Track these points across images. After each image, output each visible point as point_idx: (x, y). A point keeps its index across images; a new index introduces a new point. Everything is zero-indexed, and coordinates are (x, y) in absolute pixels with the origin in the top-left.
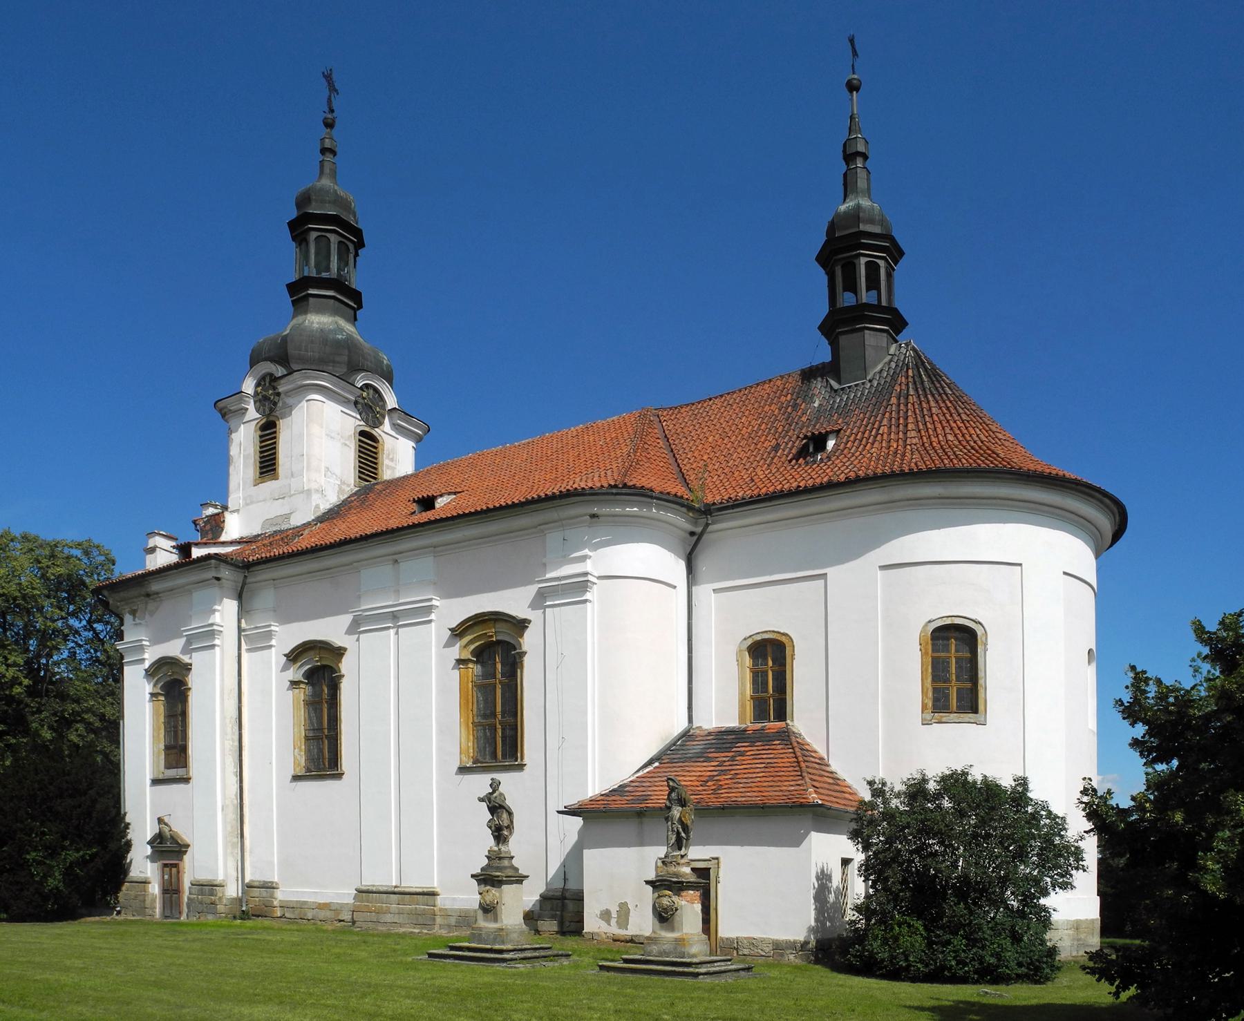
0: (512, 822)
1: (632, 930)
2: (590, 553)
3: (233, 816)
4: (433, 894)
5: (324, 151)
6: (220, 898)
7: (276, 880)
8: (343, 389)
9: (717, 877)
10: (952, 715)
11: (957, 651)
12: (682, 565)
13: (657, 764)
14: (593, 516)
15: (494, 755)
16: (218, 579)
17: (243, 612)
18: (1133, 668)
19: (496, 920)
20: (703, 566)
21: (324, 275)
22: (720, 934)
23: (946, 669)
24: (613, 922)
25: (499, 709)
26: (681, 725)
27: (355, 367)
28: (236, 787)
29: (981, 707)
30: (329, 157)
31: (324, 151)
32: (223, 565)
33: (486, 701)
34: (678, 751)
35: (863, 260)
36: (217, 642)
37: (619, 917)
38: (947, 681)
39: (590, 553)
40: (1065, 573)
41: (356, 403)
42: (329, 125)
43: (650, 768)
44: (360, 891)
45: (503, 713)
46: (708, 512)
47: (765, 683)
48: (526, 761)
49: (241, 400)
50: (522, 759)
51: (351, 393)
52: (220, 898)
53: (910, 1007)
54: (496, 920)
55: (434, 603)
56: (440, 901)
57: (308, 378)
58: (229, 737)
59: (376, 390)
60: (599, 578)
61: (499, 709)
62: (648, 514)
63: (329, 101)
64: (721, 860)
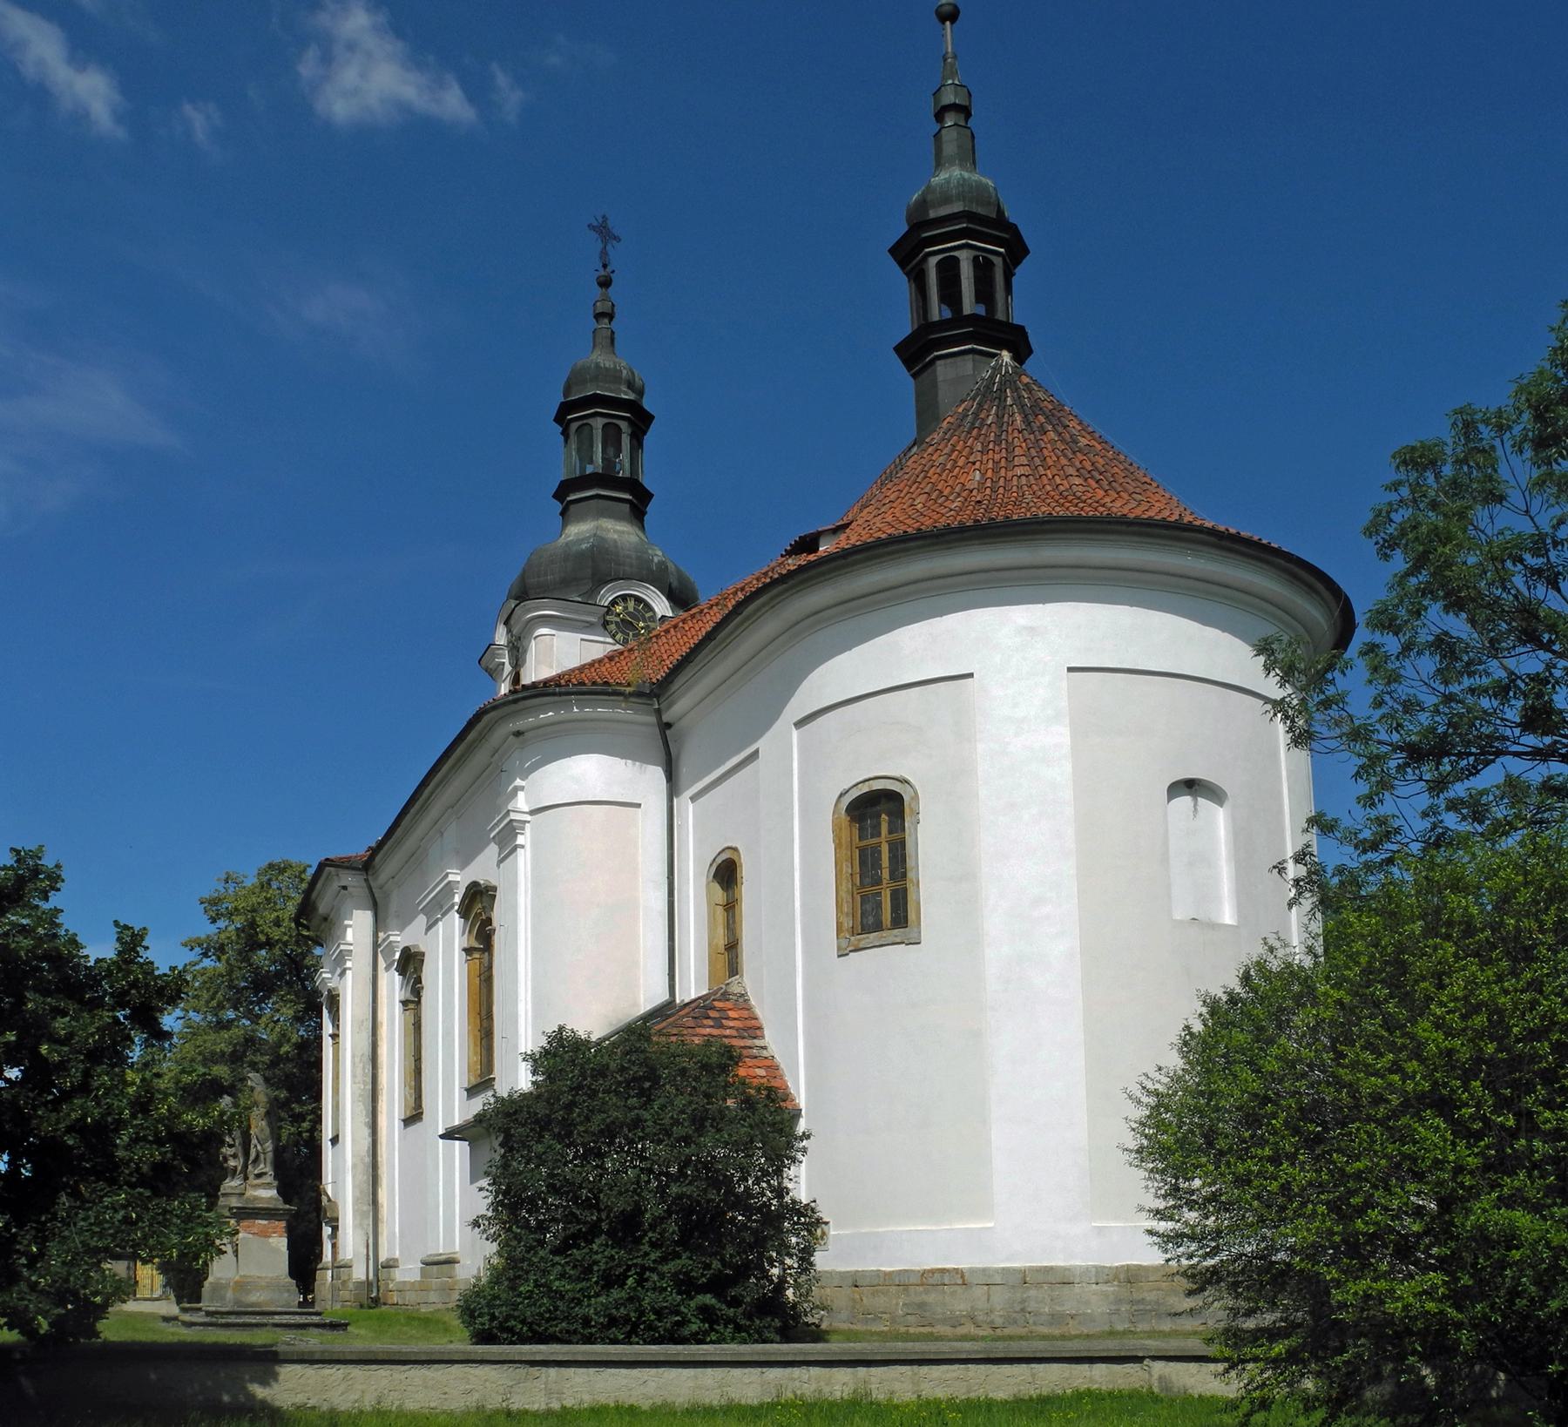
2: (523, 783)
3: (365, 1178)
4: (451, 1261)
5: (598, 316)
6: (344, 1282)
7: (397, 1255)
8: (576, 612)
10: (884, 934)
11: (890, 832)
12: (656, 774)
14: (518, 734)
16: (345, 888)
17: (379, 924)
18: (116, 923)
20: (684, 770)
21: (589, 469)
23: (877, 864)
26: (664, 997)
27: (601, 580)
28: (366, 1142)
29: (912, 916)
30: (605, 322)
31: (598, 316)
32: (342, 873)
35: (933, 261)
36: (349, 964)
38: (878, 881)
39: (523, 783)
40: (1070, 670)
41: (605, 624)
42: (605, 283)
46: (655, 693)
49: (494, 656)
51: (589, 614)
52: (344, 1282)
55: (451, 878)
57: (530, 611)
58: (359, 1078)
59: (638, 600)
60: (533, 812)
62: (568, 716)
63: (604, 253)
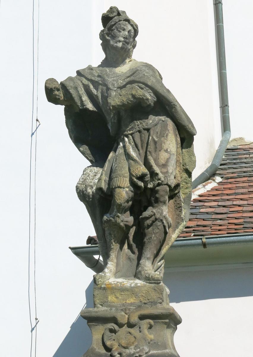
13: (218, 179)
43: (211, 185)
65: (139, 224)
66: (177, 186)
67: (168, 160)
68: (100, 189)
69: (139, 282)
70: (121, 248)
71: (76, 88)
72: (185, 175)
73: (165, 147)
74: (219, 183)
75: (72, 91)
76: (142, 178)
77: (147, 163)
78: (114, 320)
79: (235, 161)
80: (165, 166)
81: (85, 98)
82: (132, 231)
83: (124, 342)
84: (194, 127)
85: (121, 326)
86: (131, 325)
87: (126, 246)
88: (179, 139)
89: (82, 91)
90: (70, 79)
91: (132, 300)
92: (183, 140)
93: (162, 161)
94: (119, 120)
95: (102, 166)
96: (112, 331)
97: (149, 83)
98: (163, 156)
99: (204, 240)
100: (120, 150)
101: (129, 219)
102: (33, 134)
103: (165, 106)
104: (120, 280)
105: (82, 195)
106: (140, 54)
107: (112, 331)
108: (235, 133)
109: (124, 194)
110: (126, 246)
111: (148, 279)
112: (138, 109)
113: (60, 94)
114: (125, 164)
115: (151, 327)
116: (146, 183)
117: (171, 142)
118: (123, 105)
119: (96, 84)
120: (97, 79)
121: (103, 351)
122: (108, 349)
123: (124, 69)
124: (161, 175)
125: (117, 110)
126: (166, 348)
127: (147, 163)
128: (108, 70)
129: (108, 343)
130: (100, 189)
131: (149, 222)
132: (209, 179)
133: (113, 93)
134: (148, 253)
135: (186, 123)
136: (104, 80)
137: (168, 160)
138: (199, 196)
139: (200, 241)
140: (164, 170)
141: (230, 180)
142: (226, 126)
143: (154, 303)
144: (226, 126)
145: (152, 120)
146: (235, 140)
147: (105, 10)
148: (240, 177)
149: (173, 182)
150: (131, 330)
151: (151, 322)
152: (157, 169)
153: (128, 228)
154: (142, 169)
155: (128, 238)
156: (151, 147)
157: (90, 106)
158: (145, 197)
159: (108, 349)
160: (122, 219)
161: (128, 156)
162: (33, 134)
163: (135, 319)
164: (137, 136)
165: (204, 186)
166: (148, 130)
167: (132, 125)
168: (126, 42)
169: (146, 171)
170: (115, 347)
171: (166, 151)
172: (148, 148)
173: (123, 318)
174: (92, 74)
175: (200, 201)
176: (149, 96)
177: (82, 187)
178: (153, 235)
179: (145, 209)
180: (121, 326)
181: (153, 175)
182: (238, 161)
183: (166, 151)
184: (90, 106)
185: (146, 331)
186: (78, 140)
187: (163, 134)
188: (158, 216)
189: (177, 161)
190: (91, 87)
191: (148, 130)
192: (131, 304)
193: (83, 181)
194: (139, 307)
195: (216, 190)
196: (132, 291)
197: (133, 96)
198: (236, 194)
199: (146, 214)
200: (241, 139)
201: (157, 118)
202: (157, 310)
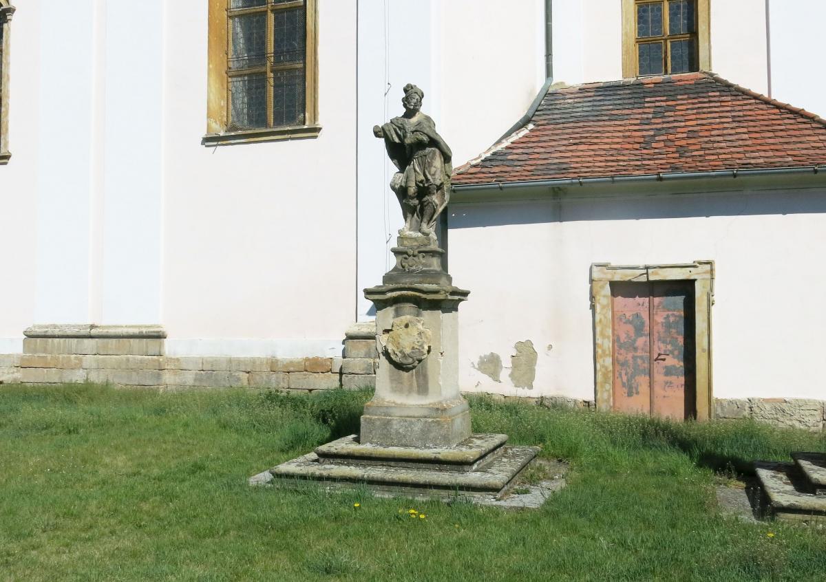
0: (51, 325)
1: (544, 385)
4: (159, 336)
9: (710, 295)
13: (531, 126)
15: (262, 121)
19: (423, 389)
22: (717, 394)
24: (505, 374)
25: (271, 48)
33: (248, 39)
34: (549, 110)
37: (515, 366)
43: (524, 132)
44: (30, 336)
45: (277, 53)
47: (658, 21)
48: (320, 123)
50: (315, 118)
53: (185, 370)
54: (423, 389)
56: (171, 348)
61: (271, 48)
64: (717, 267)
65: (421, 203)
66: (442, 184)
67: (435, 172)
68: (401, 186)
69: (420, 234)
70: (413, 216)
71: (389, 131)
72: (447, 177)
73: (434, 165)
74: (532, 131)
75: (387, 132)
76: (421, 182)
77: (425, 175)
78: (406, 253)
79: (550, 107)
80: (434, 175)
81: (394, 136)
82: (419, 207)
83: (410, 264)
84: (451, 152)
85: (409, 256)
86: (414, 256)
87: (415, 215)
88: (443, 160)
89: (393, 132)
90: (387, 124)
91: (415, 244)
92: (445, 159)
93: (432, 172)
94: (412, 149)
95: (403, 173)
96: (406, 258)
97: (426, 132)
98: (433, 170)
99: (501, 185)
100: (412, 166)
101: (416, 202)
102: (386, 94)
103: (434, 142)
104: (411, 233)
105: (393, 188)
106: (424, 110)
107: (406, 258)
108: (557, 78)
109: (412, 190)
110: (415, 215)
111: (424, 233)
112: (420, 145)
113: (382, 134)
114: (413, 174)
115: (424, 257)
116: (424, 185)
117: (438, 162)
118: (412, 143)
119: (400, 128)
120: (400, 126)
121: (401, 268)
122: (403, 267)
123: (414, 120)
124: (431, 180)
125: (411, 145)
126: (430, 267)
127: (425, 175)
128: (406, 120)
129: (404, 264)
130: (401, 186)
131: (426, 203)
132: (522, 127)
133: (408, 135)
134: (425, 220)
135: (446, 151)
136: (404, 126)
137: (435, 172)
138: (512, 143)
139: (497, 185)
140: (433, 177)
141: (540, 128)
142: (549, 73)
143: (426, 245)
144: (549, 73)
145: (428, 150)
146: (557, 84)
147: (405, 86)
148: (548, 124)
149: (438, 182)
150: (415, 258)
151: (424, 254)
152: (429, 177)
153: (415, 207)
154: (422, 177)
155: (416, 210)
156: (427, 166)
157: (397, 140)
158: (423, 191)
159: (403, 267)
160: (414, 200)
161: (415, 171)
162: (386, 94)
163: (416, 253)
164: (420, 159)
165: (517, 134)
166: (426, 156)
167: (417, 153)
168: (416, 105)
169: (424, 178)
170: (407, 266)
171: (435, 167)
172: (425, 166)
173: (410, 252)
174: (397, 122)
175: (510, 148)
176: (425, 139)
177: (393, 185)
178: (428, 211)
179: (425, 196)
180: (409, 256)
181: (427, 180)
182: (553, 107)
183: (435, 167)
184: (397, 140)
185: (421, 259)
186: (392, 156)
187: (433, 158)
188: (430, 201)
189: (441, 171)
190: (398, 130)
191: (426, 156)
192: (415, 246)
193: (393, 181)
194: (418, 247)
195: (527, 137)
196: (415, 239)
197: (417, 139)
198: (539, 142)
199: (425, 199)
200: (562, 83)
201: (430, 149)
202: (428, 248)
